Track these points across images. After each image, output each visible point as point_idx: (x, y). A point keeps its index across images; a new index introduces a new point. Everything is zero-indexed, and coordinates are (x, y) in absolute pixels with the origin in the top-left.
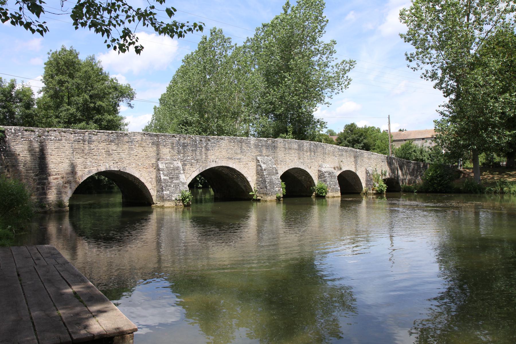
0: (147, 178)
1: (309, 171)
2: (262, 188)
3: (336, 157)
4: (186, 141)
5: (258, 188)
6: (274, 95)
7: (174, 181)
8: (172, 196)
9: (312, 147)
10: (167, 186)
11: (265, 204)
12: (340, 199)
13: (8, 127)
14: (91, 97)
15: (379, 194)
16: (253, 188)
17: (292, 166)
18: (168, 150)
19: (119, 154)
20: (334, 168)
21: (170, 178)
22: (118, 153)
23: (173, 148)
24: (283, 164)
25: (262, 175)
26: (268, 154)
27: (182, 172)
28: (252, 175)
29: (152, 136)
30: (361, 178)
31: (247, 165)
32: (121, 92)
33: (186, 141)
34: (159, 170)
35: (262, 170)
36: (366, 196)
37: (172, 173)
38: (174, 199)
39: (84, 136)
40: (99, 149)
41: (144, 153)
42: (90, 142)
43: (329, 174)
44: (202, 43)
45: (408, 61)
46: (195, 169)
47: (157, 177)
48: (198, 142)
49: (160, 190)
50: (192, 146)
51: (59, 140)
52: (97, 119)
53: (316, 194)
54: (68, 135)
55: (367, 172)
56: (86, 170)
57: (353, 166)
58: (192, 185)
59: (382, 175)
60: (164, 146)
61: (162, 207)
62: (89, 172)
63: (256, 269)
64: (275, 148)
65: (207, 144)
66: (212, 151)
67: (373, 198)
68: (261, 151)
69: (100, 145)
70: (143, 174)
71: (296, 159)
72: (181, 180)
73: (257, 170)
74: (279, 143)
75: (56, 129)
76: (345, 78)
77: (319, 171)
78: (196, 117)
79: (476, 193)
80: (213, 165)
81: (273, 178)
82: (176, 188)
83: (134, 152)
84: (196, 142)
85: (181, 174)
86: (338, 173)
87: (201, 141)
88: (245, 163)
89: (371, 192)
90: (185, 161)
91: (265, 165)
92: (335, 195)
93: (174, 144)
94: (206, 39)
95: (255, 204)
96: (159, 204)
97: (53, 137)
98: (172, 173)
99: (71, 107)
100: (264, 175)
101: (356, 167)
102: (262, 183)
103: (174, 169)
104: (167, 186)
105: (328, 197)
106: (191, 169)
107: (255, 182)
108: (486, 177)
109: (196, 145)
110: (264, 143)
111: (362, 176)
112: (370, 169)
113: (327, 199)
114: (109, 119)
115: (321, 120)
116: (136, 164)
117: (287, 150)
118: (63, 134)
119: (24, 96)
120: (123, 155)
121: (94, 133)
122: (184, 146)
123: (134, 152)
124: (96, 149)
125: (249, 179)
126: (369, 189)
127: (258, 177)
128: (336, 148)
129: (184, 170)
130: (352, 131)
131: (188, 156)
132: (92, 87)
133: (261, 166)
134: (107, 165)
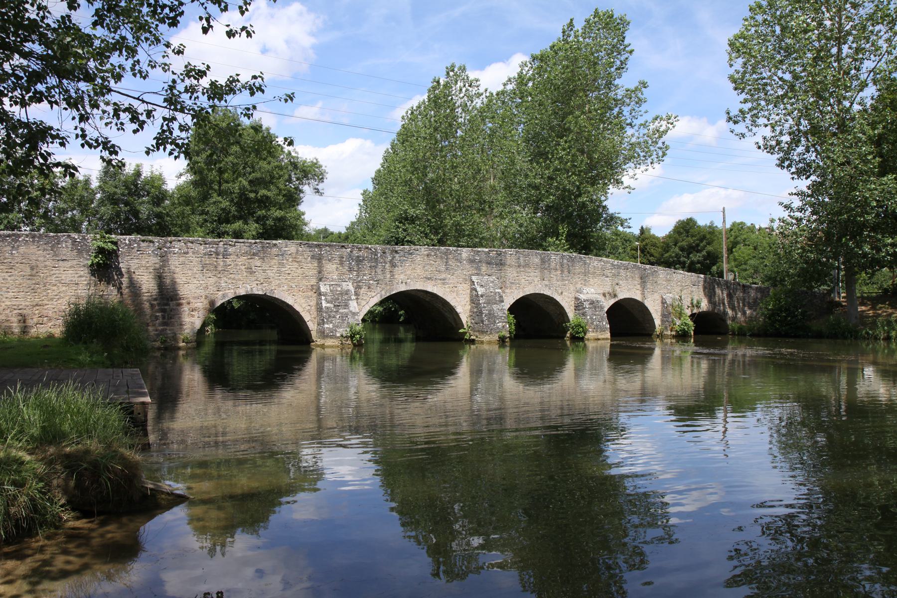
0: (304, 305)
1: (558, 298)
3: (607, 277)
4: (361, 253)
6: (537, 175)
7: (340, 311)
8: (336, 331)
9: (565, 261)
10: (330, 316)
12: (608, 343)
13: (121, 237)
14: (251, 182)
15: (682, 336)
16: (464, 322)
17: (529, 290)
18: (335, 266)
19: (264, 271)
20: (604, 295)
21: (335, 306)
23: (342, 263)
24: (514, 288)
25: (477, 304)
26: (489, 272)
27: (353, 297)
28: (463, 303)
29: (311, 247)
30: (652, 310)
31: (455, 289)
32: (304, 171)
33: (361, 253)
34: (320, 294)
35: (477, 296)
36: (662, 340)
37: (338, 299)
38: (338, 335)
39: (217, 248)
40: (237, 265)
41: (300, 271)
42: (225, 255)
43: (590, 304)
44: (434, 88)
45: (731, 122)
46: (374, 294)
47: (317, 304)
48: (379, 255)
49: (321, 323)
50: (371, 260)
51: (184, 253)
52: (260, 216)
54: (196, 247)
55: (663, 302)
56: (220, 293)
57: (639, 292)
58: (371, 318)
59: (693, 306)
61: (323, 346)
62: (224, 296)
63: (680, 518)
64: (501, 264)
66: (400, 268)
68: (478, 269)
70: (298, 300)
72: (351, 309)
73: (471, 296)
74: (508, 257)
75: (180, 238)
76: (660, 145)
77: (575, 298)
78: (421, 209)
79: (845, 338)
80: (403, 288)
81: (495, 309)
82: (342, 320)
85: (351, 300)
86: (608, 303)
88: (452, 285)
89: (669, 333)
90: (359, 282)
91: (483, 289)
92: (600, 337)
94: (438, 82)
96: (319, 342)
97: (177, 250)
98: (338, 299)
99: (222, 198)
100: (481, 304)
101: (643, 294)
103: (341, 294)
104: (330, 316)
105: (588, 340)
106: (369, 293)
107: (468, 314)
108: (880, 312)
110: (483, 256)
114: (277, 217)
115: (617, 215)
116: (288, 285)
118: (190, 244)
119: (153, 187)
120: (270, 274)
122: (359, 260)
125: (459, 310)
126: (666, 328)
127: (472, 307)
128: (608, 262)
129: (356, 294)
130: (687, 232)
131: (364, 275)
132: (253, 167)
133: (476, 291)
134: (248, 286)
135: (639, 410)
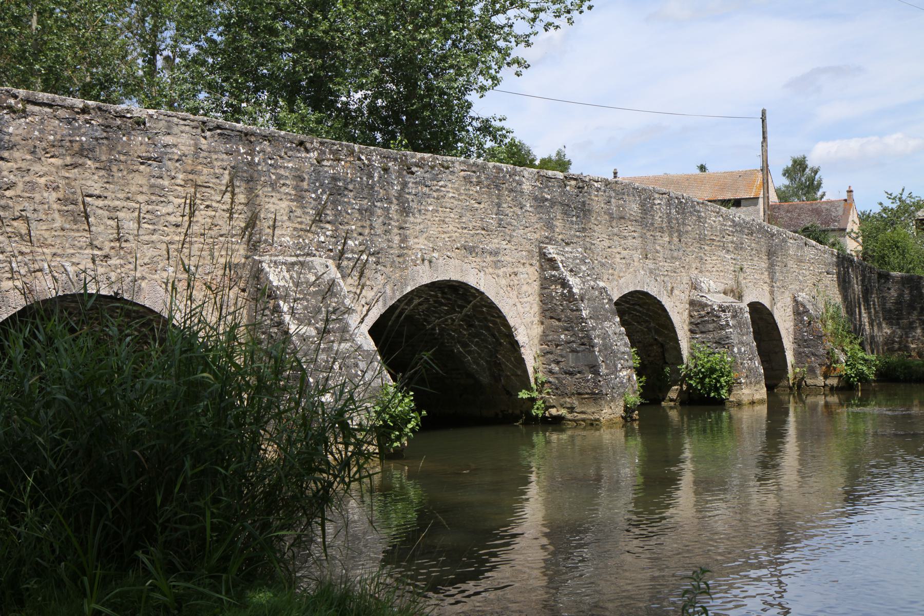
2: (571, 374)
5: (551, 372)
11: (591, 436)
18: (284, 204)
22: (108, 208)
23: (299, 198)
25: (570, 320)
36: (800, 399)
53: (681, 392)
60: (273, 185)
65: (405, 185)
67: (827, 405)
69: (36, 167)
71: (637, 255)
83: (170, 208)
84: (372, 177)
87: (386, 170)
88: (509, 270)
89: (820, 381)
93: (303, 180)
95: (538, 439)
101: (772, 293)
102: (573, 351)
105: (739, 404)
109: (372, 188)
111: (787, 326)
112: (803, 297)
113: (733, 411)
117: (614, 224)
121: (12, 101)
122: (337, 190)
123: (170, 208)
124: (20, 186)
126: (812, 370)
133: (564, 284)
135: (733, 568)
